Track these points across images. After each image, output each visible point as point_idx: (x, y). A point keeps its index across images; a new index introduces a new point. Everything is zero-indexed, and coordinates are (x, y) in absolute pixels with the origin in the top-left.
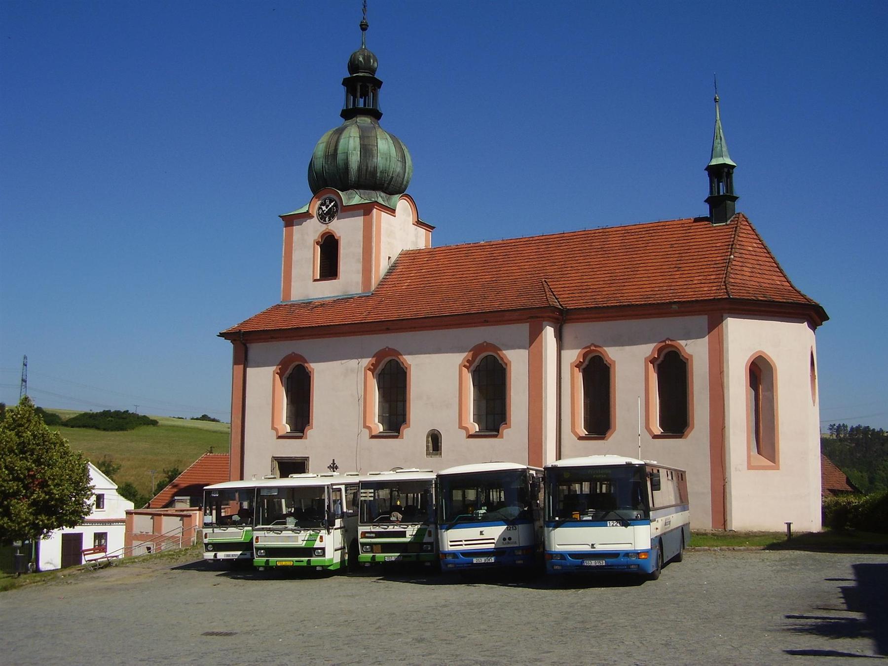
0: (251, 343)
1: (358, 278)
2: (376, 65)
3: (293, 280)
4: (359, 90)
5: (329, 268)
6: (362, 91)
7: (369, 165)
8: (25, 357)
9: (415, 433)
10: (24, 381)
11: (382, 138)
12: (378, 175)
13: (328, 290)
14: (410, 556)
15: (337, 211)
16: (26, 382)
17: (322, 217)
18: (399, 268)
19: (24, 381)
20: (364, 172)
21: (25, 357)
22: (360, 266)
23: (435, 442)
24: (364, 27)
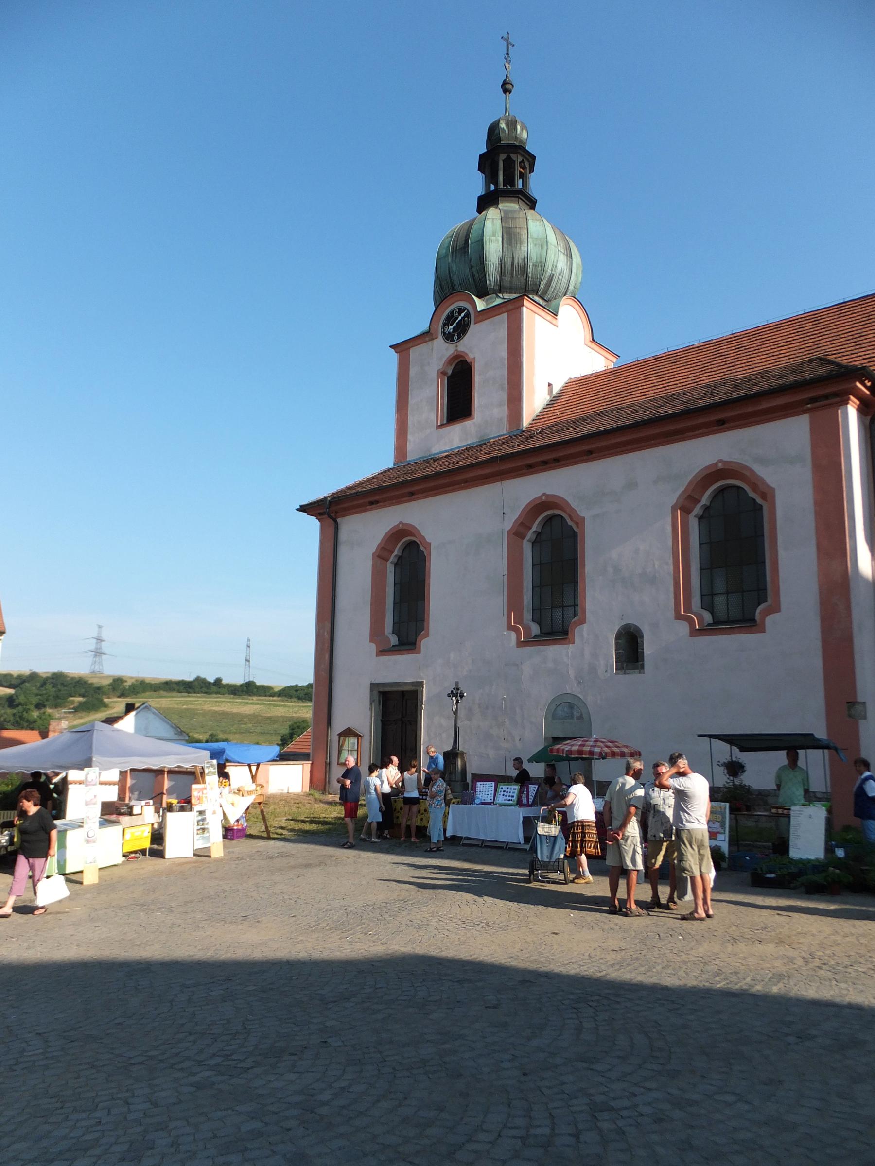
0: (343, 516)
1: (500, 412)
2: (525, 135)
3: (410, 431)
4: (662, 853)
5: (458, 406)
6: (505, 168)
7: (516, 256)
8: (249, 640)
9: (595, 639)
10: (248, 660)
11: (534, 220)
12: (530, 270)
13: (457, 437)
14: (233, 852)
15: (469, 322)
16: (249, 661)
17: (449, 338)
18: (564, 399)
19: (248, 660)
20: (508, 261)
21: (249, 640)
22: (504, 396)
23: (630, 648)
24: (506, 87)
